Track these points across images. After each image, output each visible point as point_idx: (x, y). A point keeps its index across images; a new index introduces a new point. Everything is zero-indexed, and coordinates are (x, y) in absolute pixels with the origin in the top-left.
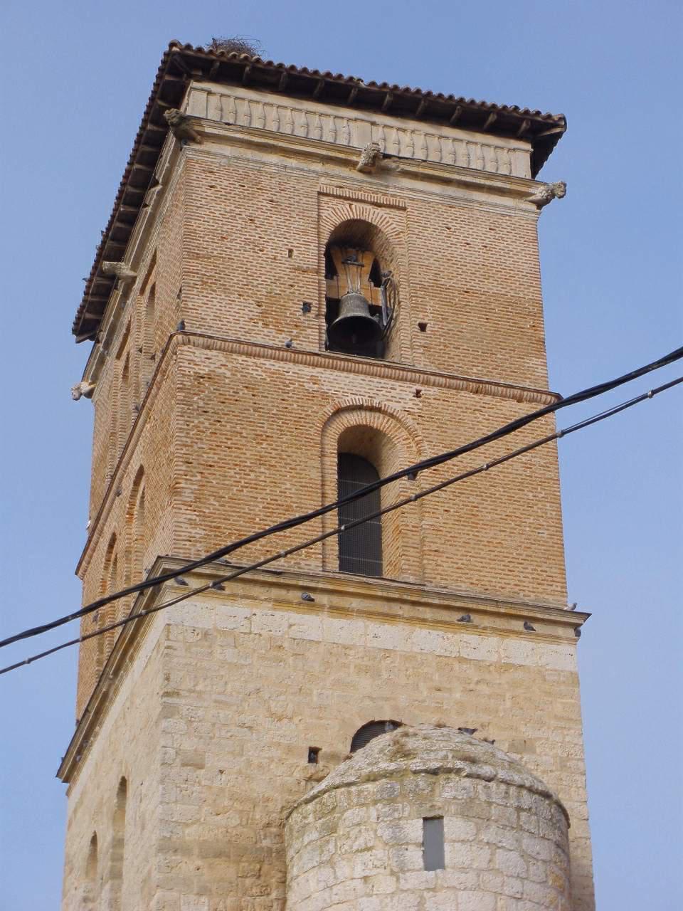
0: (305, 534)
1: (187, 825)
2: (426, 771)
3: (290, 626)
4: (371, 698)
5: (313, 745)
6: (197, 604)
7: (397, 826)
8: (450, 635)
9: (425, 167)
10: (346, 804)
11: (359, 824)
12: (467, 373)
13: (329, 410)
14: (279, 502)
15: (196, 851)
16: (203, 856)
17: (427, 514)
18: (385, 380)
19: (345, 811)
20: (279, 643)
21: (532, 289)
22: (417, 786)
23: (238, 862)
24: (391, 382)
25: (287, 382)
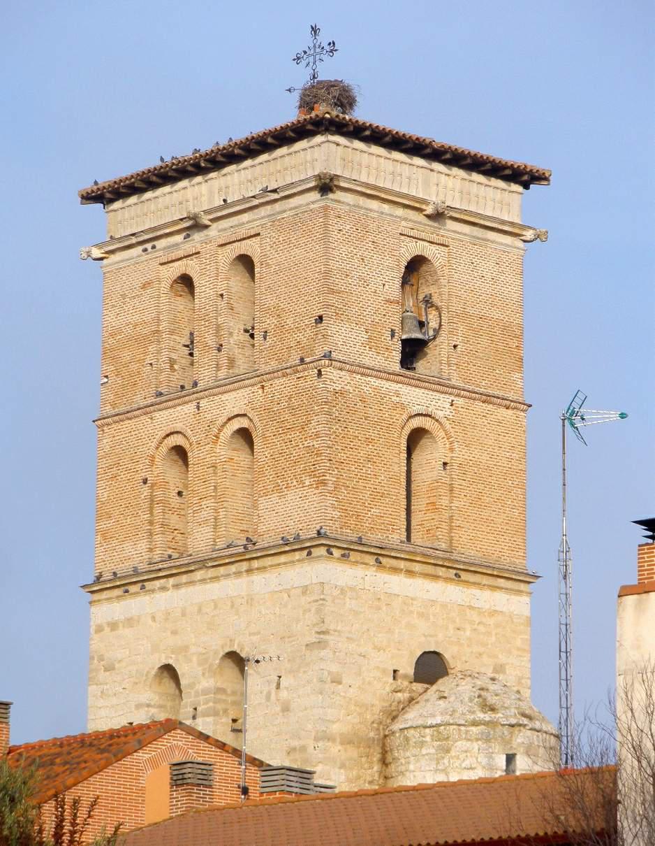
0: (391, 515)
1: (333, 722)
2: (509, 725)
3: (385, 583)
4: (424, 635)
5: (395, 669)
6: (338, 568)
7: (491, 757)
8: (465, 590)
9: (465, 214)
10: (457, 737)
11: (466, 752)
12: (478, 386)
13: (405, 417)
14: (378, 490)
15: (338, 740)
16: (342, 744)
17: (455, 499)
18: (435, 393)
19: (456, 741)
20: (379, 597)
21: (518, 314)
22: (503, 733)
23: (359, 747)
24: (438, 394)
25: (383, 395)
